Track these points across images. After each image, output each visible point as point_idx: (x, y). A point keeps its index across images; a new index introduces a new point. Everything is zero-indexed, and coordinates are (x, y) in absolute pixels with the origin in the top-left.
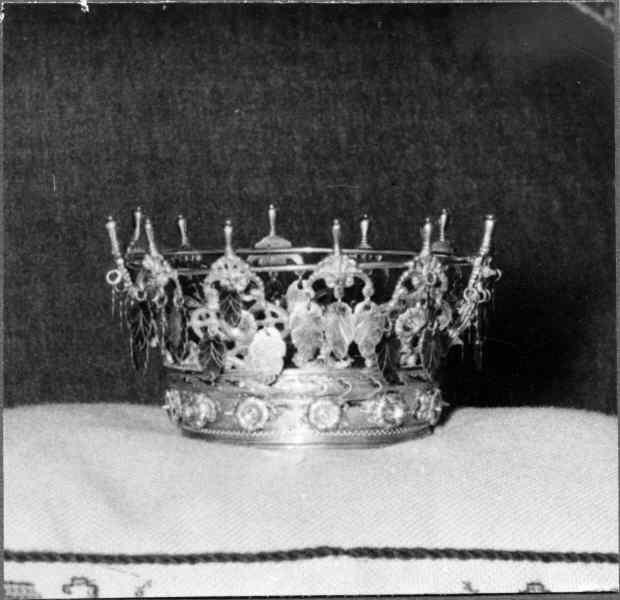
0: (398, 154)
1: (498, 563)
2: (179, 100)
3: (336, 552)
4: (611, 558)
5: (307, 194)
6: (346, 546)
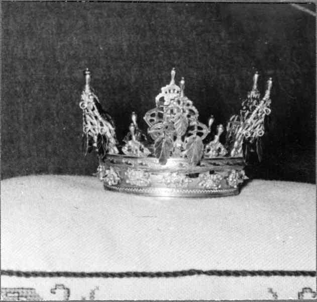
0: (154, 57)
1: (287, 278)
2: (39, 28)
3: (199, 272)
4: (312, 274)
5: (106, 77)
6: (205, 269)
